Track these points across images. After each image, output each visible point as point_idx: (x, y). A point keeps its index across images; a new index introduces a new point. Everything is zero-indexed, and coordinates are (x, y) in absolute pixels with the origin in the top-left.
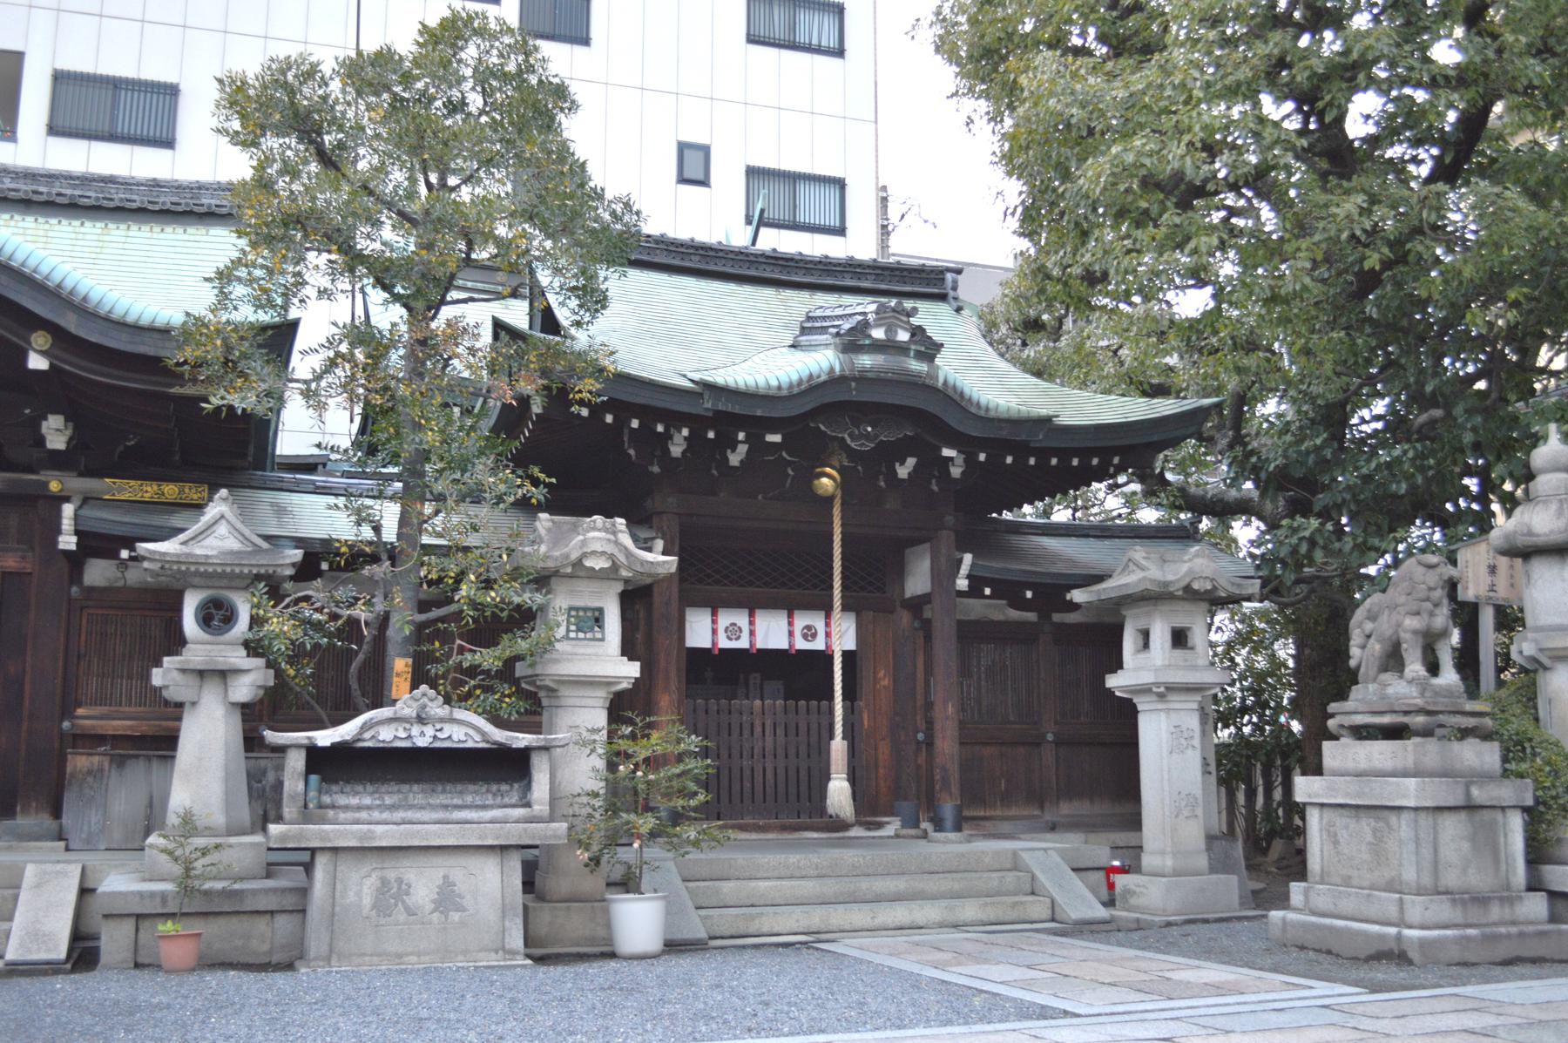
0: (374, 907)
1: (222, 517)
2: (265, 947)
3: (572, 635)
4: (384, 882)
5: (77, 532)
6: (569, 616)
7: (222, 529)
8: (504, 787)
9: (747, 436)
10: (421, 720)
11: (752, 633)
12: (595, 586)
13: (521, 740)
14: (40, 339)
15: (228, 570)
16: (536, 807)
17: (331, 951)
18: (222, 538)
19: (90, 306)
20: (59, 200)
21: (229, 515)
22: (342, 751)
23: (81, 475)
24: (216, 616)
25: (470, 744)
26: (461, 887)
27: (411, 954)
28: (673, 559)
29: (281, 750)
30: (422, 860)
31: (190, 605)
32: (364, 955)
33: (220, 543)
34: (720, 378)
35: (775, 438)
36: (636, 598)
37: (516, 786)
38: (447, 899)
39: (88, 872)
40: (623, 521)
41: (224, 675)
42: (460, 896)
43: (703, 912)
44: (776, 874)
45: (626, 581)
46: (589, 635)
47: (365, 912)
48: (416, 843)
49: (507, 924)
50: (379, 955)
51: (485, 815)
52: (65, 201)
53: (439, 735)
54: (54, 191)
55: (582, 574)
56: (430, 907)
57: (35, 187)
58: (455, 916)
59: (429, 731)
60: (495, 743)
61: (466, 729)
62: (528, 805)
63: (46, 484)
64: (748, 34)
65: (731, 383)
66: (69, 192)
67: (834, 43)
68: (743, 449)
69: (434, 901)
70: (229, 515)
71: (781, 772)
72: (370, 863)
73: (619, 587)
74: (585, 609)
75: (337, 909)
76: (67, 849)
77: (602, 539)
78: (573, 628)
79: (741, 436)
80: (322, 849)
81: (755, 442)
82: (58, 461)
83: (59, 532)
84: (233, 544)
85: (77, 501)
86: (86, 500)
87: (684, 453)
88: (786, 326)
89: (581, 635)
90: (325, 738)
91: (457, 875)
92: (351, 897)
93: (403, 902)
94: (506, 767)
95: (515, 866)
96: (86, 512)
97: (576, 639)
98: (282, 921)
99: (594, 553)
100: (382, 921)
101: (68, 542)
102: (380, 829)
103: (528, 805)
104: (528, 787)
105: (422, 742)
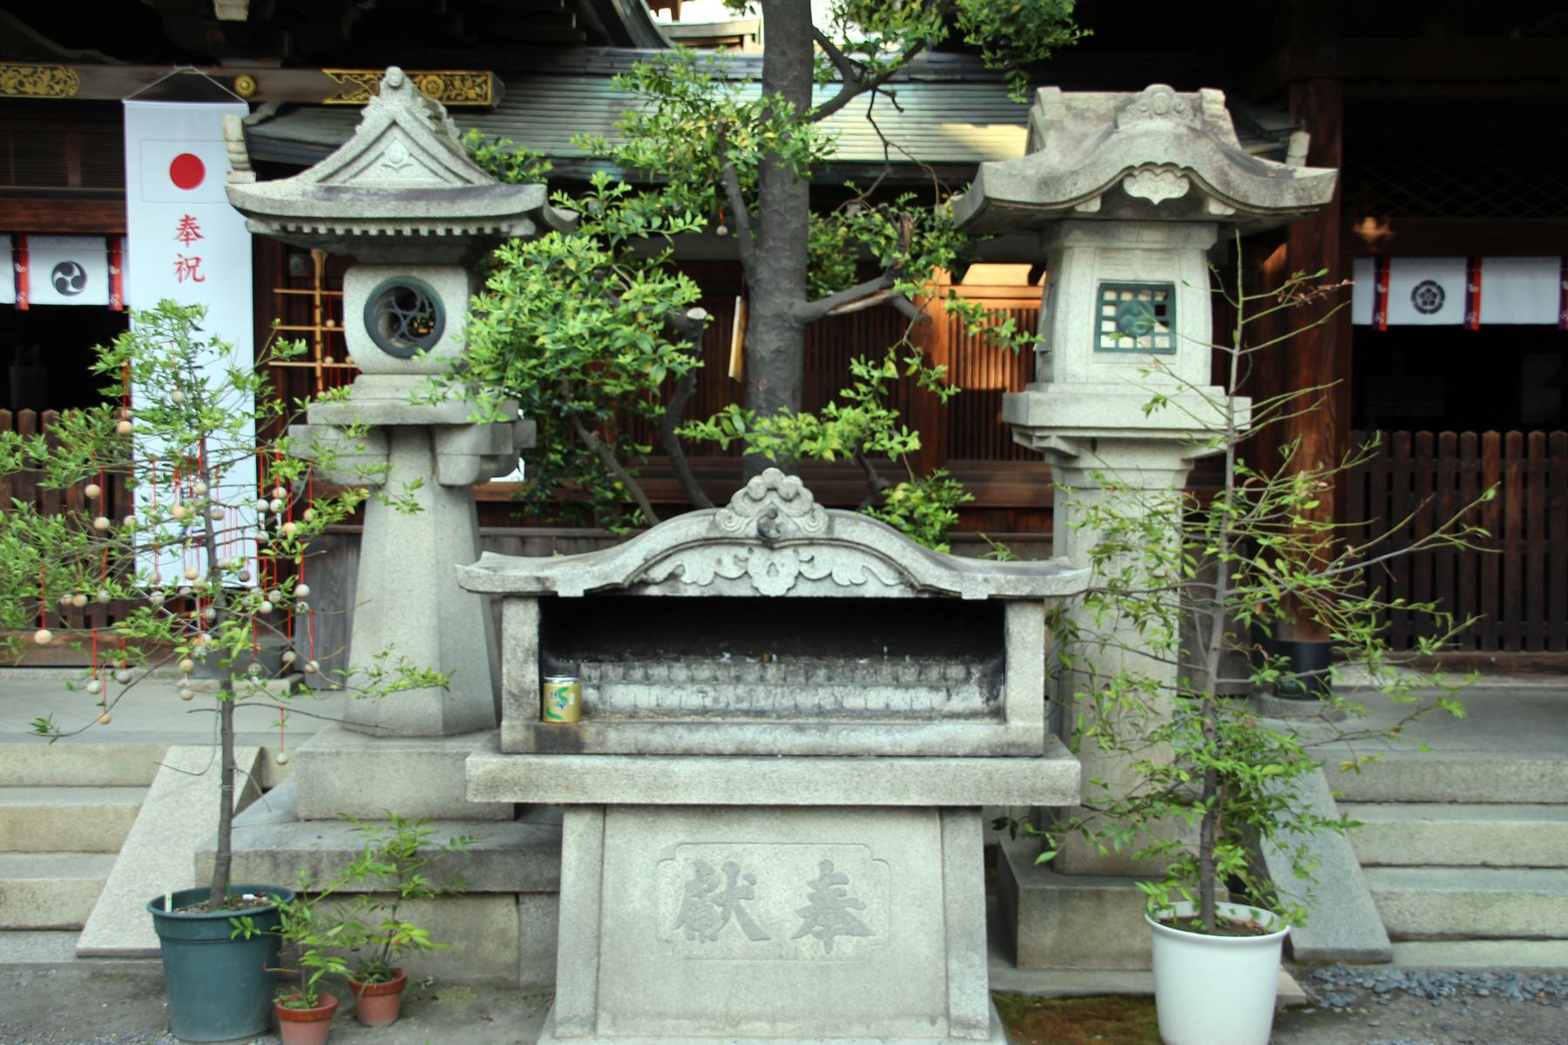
0: (681, 921)
1: (394, 123)
2: (509, 956)
3: (1106, 342)
4: (702, 870)
6: (1101, 302)
7: (396, 147)
8: (956, 671)
10: (766, 541)
11: (1472, 302)
13: (976, 578)
15: (373, 231)
17: (596, 1005)
18: (397, 167)
23: (288, 64)
24: (407, 320)
25: (872, 590)
26: (856, 887)
27: (759, 1017)
28: (1328, 173)
29: (992, 613)
31: (357, 293)
32: (662, 1015)
36: (1245, 254)
37: (976, 672)
38: (829, 910)
41: (428, 435)
42: (855, 903)
43: (1381, 881)
44: (1533, 795)
45: (1223, 224)
46: (1144, 342)
47: (666, 928)
49: (954, 965)
50: (694, 1016)
51: (914, 725)
53: (805, 569)
55: (1126, 213)
56: (794, 923)
58: (847, 945)
60: (927, 588)
61: (863, 560)
62: (999, 714)
69: (802, 913)
71: (1535, 565)
72: (675, 832)
73: (1207, 239)
74: (1136, 288)
75: (608, 922)
78: (1109, 326)
84: (419, 177)
89: (1126, 342)
90: (574, 576)
91: (847, 863)
92: (636, 901)
93: (741, 913)
94: (958, 633)
95: (970, 839)
97: (1117, 350)
98: (531, 906)
99: (1148, 166)
100: (698, 948)
102: (684, 767)
103: (999, 714)
104: (996, 678)
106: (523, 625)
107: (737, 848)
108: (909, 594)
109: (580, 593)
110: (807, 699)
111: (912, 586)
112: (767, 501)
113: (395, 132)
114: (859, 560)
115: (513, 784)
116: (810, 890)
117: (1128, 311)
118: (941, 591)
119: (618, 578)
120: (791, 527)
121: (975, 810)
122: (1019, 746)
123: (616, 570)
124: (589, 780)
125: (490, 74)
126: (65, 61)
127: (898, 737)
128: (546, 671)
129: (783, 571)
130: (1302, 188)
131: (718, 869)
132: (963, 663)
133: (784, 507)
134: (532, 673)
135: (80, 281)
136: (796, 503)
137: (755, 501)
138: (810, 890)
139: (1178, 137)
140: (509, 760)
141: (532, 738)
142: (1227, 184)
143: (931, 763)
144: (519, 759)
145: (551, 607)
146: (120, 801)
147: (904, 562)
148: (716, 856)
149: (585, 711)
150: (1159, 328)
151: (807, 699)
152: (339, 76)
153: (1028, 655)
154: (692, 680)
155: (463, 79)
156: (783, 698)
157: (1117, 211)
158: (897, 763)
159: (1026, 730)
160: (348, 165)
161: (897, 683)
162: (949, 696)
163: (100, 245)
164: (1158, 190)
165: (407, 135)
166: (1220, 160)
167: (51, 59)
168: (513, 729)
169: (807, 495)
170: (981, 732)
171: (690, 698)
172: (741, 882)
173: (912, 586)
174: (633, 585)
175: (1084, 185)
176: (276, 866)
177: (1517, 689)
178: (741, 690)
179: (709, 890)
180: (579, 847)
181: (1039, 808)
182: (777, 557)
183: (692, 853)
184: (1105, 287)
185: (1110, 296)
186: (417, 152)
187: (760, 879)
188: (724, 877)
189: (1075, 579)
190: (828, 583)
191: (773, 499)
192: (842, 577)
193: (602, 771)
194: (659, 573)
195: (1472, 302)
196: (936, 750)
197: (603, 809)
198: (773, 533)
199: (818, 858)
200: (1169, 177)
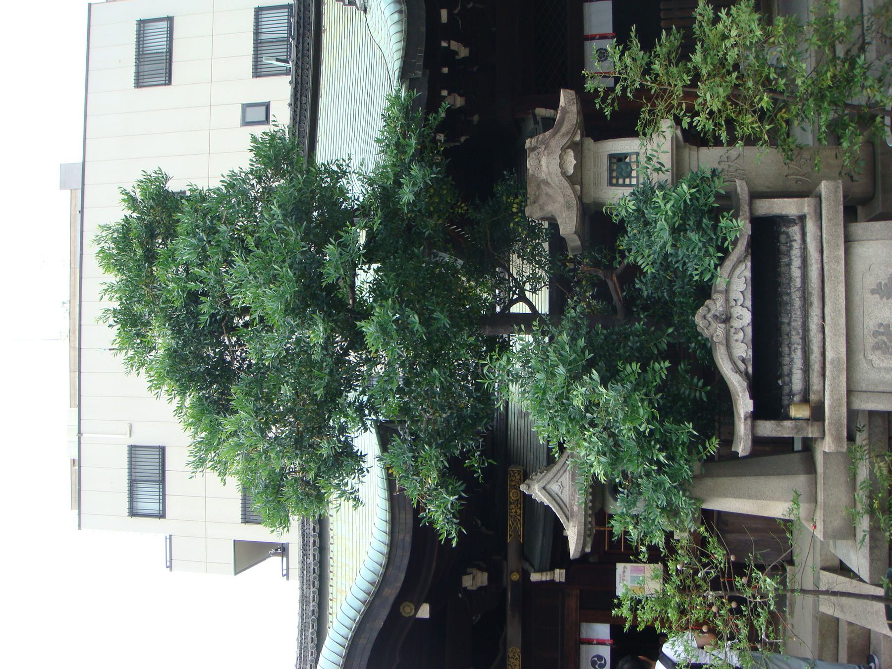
1: (544, 488)
4: (876, 347)
5: (552, 569)
6: (617, 185)
7: (554, 487)
8: (783, 238)
9: (444, 40)
10: (726, 319)
11: (603, 37)
12: (589, 163)
14: (407, 610)
16: (806, 210)
19: (377, 579)
20: (318, 530)
21: (542, 483)
22: (755, 391)
25: (748, 274)
30: (857, 313)
33: (567, 489)
34: (394, 64)
35: (444, 13)
39: (828, 564)
40: (528, 142)
48: (843, 321)
52: (318, 527)
53: (739, 303)
54: (312, 533)
57: (311, 545)
59: (737, 311)
60: (746, 250)
61: (736, 282)
62: (802, 218)
63: (514, 584)
64: (165, 85)
65: (398, 55)
66: (312, 525)
67: (164, 24)
68: (454, 45)
70: (542, 483)
73: (589, 142)
74: (611, 171)
76: (791, 562)
77: (548, 163)
78: (627, 181)
79: (444, 44)
80: (849, 403)
81: (449, 32)
82: (496, 576)
83: (552, 581)
85: (527, 566)
86: (524, 554)
87: (460, 95)
88: (351, 20)
89: (634, 174)
90: (744, 404)
94: (768, 245)
95: (861, 228)
96: (537, 562)
99: (561, 166)
101: (559, 575)
102: (829, 355)
103: (802, 218)
105: (747, 317)
106: (768, 428)
107: (866, 331)
108: (749, 258)
109: (751, 401)
110: (797, 303)
111: (746, 256)
112: (710, 319)
113: (548, 487)
114: (735, 279)
115: (838, 430)
116: (884, 299)
117: (621, 173)
118: (748, 244)
119: (745, 384)
120: (721, 309)
121: (846, 227)
122: (816, 208)
123: (741, 386)
124: (836, 397)
125: (509, 469)
126: (505, 652)
127: (813, 261)
128: (788, 417)
129: (741, 313)
130: (568, 102)
131: (876, 340)
132: (779, 236)
133: (713, 312)
134: (787, 424)
135: (600, 658)
136: (710, 307)
137: (710, 324)
138: (884, 299)
139: (549, 154)
140: (827, 432)
141: (816, 423)
142: (568, 133)
143: (825, 246)
144: (826, 428)
145: (757, 415)
146: (844, 631)
147: (735, 259)
148: (870, 341)
149: (805, 400)
150: (627, 160)
151: (797, 303)
152: (510, 535)
153: (775, 206)
154: (789, 355)
155: (512, 481)
156: (797, 314)
157: (575, 179)
158: (825, 260)
159: (809, 206)
160: (561, 508)
161: (789, 265)
162: (795, 240)
163: (584, 648)
164: (571, 161)
165: (549, 482)
166: (558, 137)
167: (504, 659)
168: (811, 432)
169: (707, 302)
170: (811, 226)
171: (798, 356)
172: (882, 330)
173: (746, 256)
174: (748, 379)
175: (569, 192)
176: (876, 546)
177: (778, 5)
178: (794, 333)
179: (886, 344)
180: (866, 402)
181: (844, 207)
182: (735, 315)
183: (869, 353)
184: (611, 184)
185: (614, 181)
186: (556, 479)
187: (880, 321)
188: (880, 337)
189: (741, 186)
190: (745, 293)
191: (709, 316)
192: (742, 287)
193: (832, 391)
194: (742, 366)
195: (603, 37)
196: (819, 244)
197: (850, 392)
198: (724, 317)
199: (869, 295)
200: (565, 157)
